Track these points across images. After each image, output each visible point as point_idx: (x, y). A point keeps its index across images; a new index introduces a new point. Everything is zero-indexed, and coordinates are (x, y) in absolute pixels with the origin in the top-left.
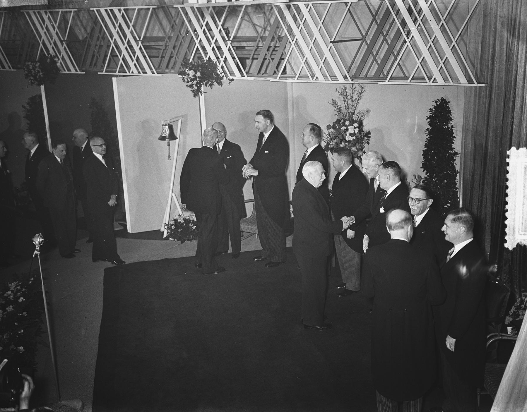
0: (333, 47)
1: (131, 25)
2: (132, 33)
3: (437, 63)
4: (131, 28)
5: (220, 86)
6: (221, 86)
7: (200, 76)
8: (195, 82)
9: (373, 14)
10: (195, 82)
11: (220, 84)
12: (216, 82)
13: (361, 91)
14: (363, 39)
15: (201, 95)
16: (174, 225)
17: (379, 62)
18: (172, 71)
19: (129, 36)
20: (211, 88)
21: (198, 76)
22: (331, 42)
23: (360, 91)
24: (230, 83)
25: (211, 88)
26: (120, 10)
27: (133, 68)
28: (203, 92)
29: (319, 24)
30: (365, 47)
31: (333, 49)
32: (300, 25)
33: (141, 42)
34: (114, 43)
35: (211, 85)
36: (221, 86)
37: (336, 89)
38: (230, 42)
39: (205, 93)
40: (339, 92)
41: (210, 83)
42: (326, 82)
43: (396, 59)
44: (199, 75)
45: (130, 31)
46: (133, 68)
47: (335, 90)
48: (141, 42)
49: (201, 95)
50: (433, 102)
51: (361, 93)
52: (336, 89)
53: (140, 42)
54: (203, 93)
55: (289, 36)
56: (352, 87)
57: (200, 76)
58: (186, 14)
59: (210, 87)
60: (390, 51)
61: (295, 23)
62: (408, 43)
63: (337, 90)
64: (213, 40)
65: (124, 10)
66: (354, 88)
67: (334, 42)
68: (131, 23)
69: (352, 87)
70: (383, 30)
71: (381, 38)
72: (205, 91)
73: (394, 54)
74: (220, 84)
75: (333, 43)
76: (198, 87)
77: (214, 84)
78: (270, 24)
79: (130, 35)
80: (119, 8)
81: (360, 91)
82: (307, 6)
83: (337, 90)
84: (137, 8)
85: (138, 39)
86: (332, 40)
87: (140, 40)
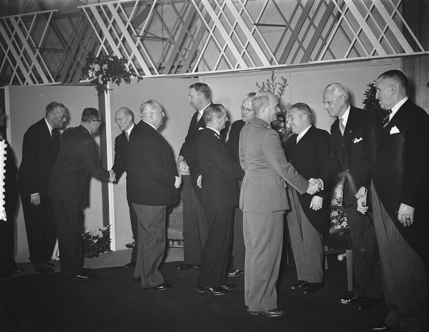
0: (257, 29)
1: (28, 33)
2: (29, 41)
3: (376, 34)
4: (29, 35)
5: (128, 83)
6: (129, 83)
7: (106, 68)
8: (101, 76)
9: (287, 22)
10: (101, 76)
11: (128, 81)
12: (123, 79)
13: (284, 84)
14: (287, 26)
15: (107, 93)
16: (120, 60)
17: (317, 25)
18: (71, 83)
19: (26, 46)
20: (118, 84)
21: (105, 69)
22: (255, 24)
23: (283, 84)
24: (139, 82)
25: (118, 84)
26: (17, 19)
27: (28, 80)
28: (109, 89)
29: (231, 29)
30: (289, 34)
31: (246, 55)
32: (219, 10)
33: (38, 49)
34: (8, 54)
35: (118, 83)
36: (129, 83)
37: (257, 83)
38: (140, 38)
39: (111, 91)
40: (259, 87)
41: (117, 79)
42: (250, 68)
43: (324, 44)
44: (106, 67)
45: (27, 39)
46: (28, 80)
47: (256, 85)
48: (38, 49)
49: (107, 93)
50: (368, 85)
51: (284, 87)
52: (257, 83)
53: (37, 50)
54: (109, 90)
55: (207, 24)
56: (272, 84)
57: (106, 68)
58: (92, 16)
59: (117, 84)
60: (317, 36)
61: (218, 2)
62: (343, 16)
63: (257, 84)
64: (120, 38)
65: (22, 17)
66: (275, 85)
67: (257, 25)
68: (28, 30)
69: (272, 84)
70: (309, 14)
71: (307, 22)
72: (110, 89)
73: (322, 38)
74: (128, 81)
75: (257, 26)
76: (104, 81)
77: (121, 81)
78: (183, 21)
79: (27, 44)
80: (16, 16)
81: (283, 84)
82: (211, 27)
83: (257, 84)
84: (36, 14)
85: (35, 46)
86: (256, 23)
87: (37, 48)
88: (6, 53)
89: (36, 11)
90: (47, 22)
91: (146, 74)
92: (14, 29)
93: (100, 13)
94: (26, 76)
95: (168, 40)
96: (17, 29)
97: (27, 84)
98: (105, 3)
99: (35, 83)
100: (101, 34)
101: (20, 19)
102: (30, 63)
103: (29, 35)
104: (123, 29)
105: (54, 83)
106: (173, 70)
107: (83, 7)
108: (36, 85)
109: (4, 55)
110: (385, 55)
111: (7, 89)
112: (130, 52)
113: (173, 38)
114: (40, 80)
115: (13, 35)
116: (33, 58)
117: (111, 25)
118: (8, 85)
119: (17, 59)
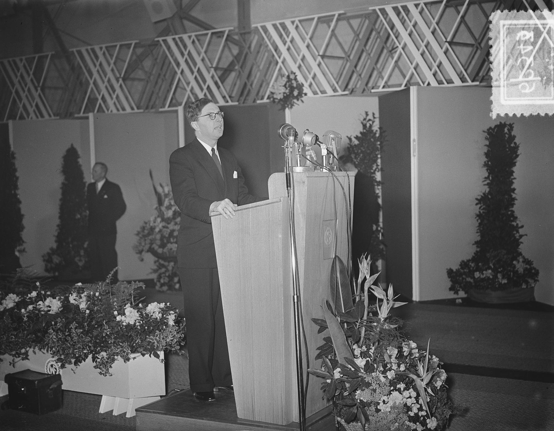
19: (200, 64)
27: (32, 115)
46: (32, 115)
88: (14, 91)
89: (259, 23)
90: (129, 52)
91: (454, 82)
92: (290, 33)
93: (177, 44)
94: (31, 110)
95: (475, 46)
96: (190, 47)
97: (32, 118)
98: (78, 49)
99: (37, 117)
100: (178, 65)
101: (104, 49)
102: (33, 99)
103: (112, 65)
104: (302, 46)
105: (470, 83)
106: (241, 98)
107: (75, 50)
108: (119, 113)
109: (11, 93)
110: (333, 93)
111: (11, 123)
112: (435, 59)
113: (349, 56)
114: (42, 116)
115: (186, 53)
116: (36, 95)
117: (289, 43)
118: (93, 111)
119: (23, 95)
